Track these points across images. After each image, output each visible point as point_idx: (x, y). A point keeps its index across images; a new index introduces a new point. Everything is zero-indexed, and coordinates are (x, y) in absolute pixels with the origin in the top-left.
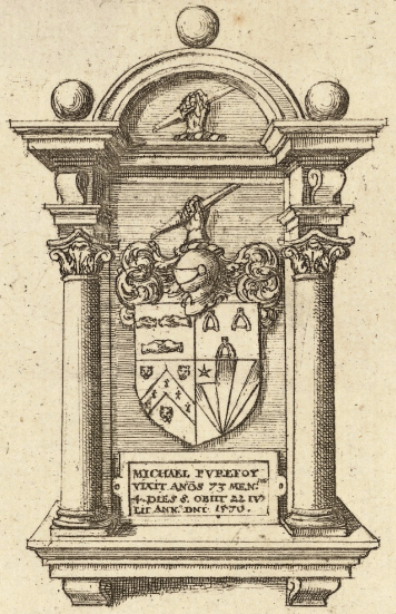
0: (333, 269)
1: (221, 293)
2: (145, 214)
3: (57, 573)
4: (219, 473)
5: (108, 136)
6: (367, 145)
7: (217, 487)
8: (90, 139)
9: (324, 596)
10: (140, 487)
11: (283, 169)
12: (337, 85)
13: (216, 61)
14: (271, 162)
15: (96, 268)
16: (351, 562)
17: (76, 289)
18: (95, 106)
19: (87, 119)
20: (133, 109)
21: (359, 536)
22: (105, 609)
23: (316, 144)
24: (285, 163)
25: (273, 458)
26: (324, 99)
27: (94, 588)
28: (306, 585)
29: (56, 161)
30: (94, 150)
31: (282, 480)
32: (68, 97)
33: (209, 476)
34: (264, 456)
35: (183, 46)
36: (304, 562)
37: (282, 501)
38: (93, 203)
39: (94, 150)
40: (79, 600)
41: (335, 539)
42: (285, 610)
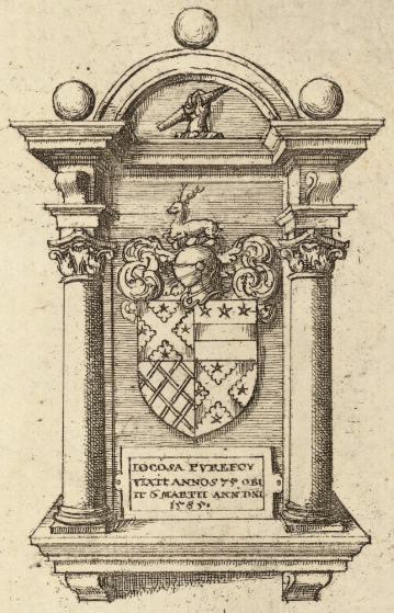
0: (333, 267)
1: (206, 281)
2: (142, 206)
3: (60, 568)
4: (213, 467)
5: (110, 138)
6: (363, 146)
7: (229, 484)
8: (83, 137)
9: (315, 593)
10: (140, 483)
11: (281, 166)
12: (336, 88)
13: (213, 63)
14: (269, 162)
15: (91, 256)
16: (346, 558)
17: (77, 292)
18: (96, 108)
19: (89, 118)
20: (130, 114)
21: (355, 535)
22: (104, 606)
23: (315, 142)
24: (282, 161)
25: (268, 454)
26: (317, 97)
27: (93, 582)
28: (118, 493)
29: (50, 159)
30: (97, 153)
31: (278, 477)
32: (73, 99)
33: (203, 470)
34: (257, 452)
35: (178, 46)
36: (305, 558)
37: (277, 497)
38: (95, 202)
39: (97, 153)
40: (81, 596)
41: (330, 536)
42: (282, 606)
